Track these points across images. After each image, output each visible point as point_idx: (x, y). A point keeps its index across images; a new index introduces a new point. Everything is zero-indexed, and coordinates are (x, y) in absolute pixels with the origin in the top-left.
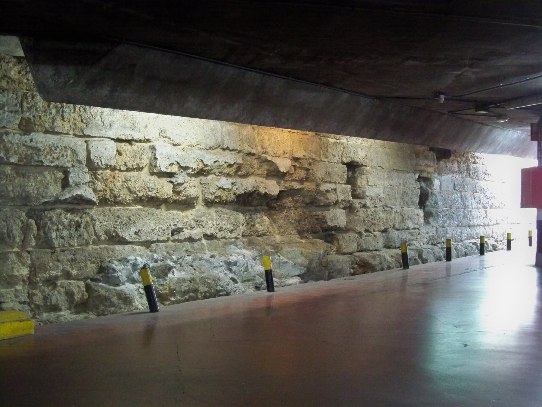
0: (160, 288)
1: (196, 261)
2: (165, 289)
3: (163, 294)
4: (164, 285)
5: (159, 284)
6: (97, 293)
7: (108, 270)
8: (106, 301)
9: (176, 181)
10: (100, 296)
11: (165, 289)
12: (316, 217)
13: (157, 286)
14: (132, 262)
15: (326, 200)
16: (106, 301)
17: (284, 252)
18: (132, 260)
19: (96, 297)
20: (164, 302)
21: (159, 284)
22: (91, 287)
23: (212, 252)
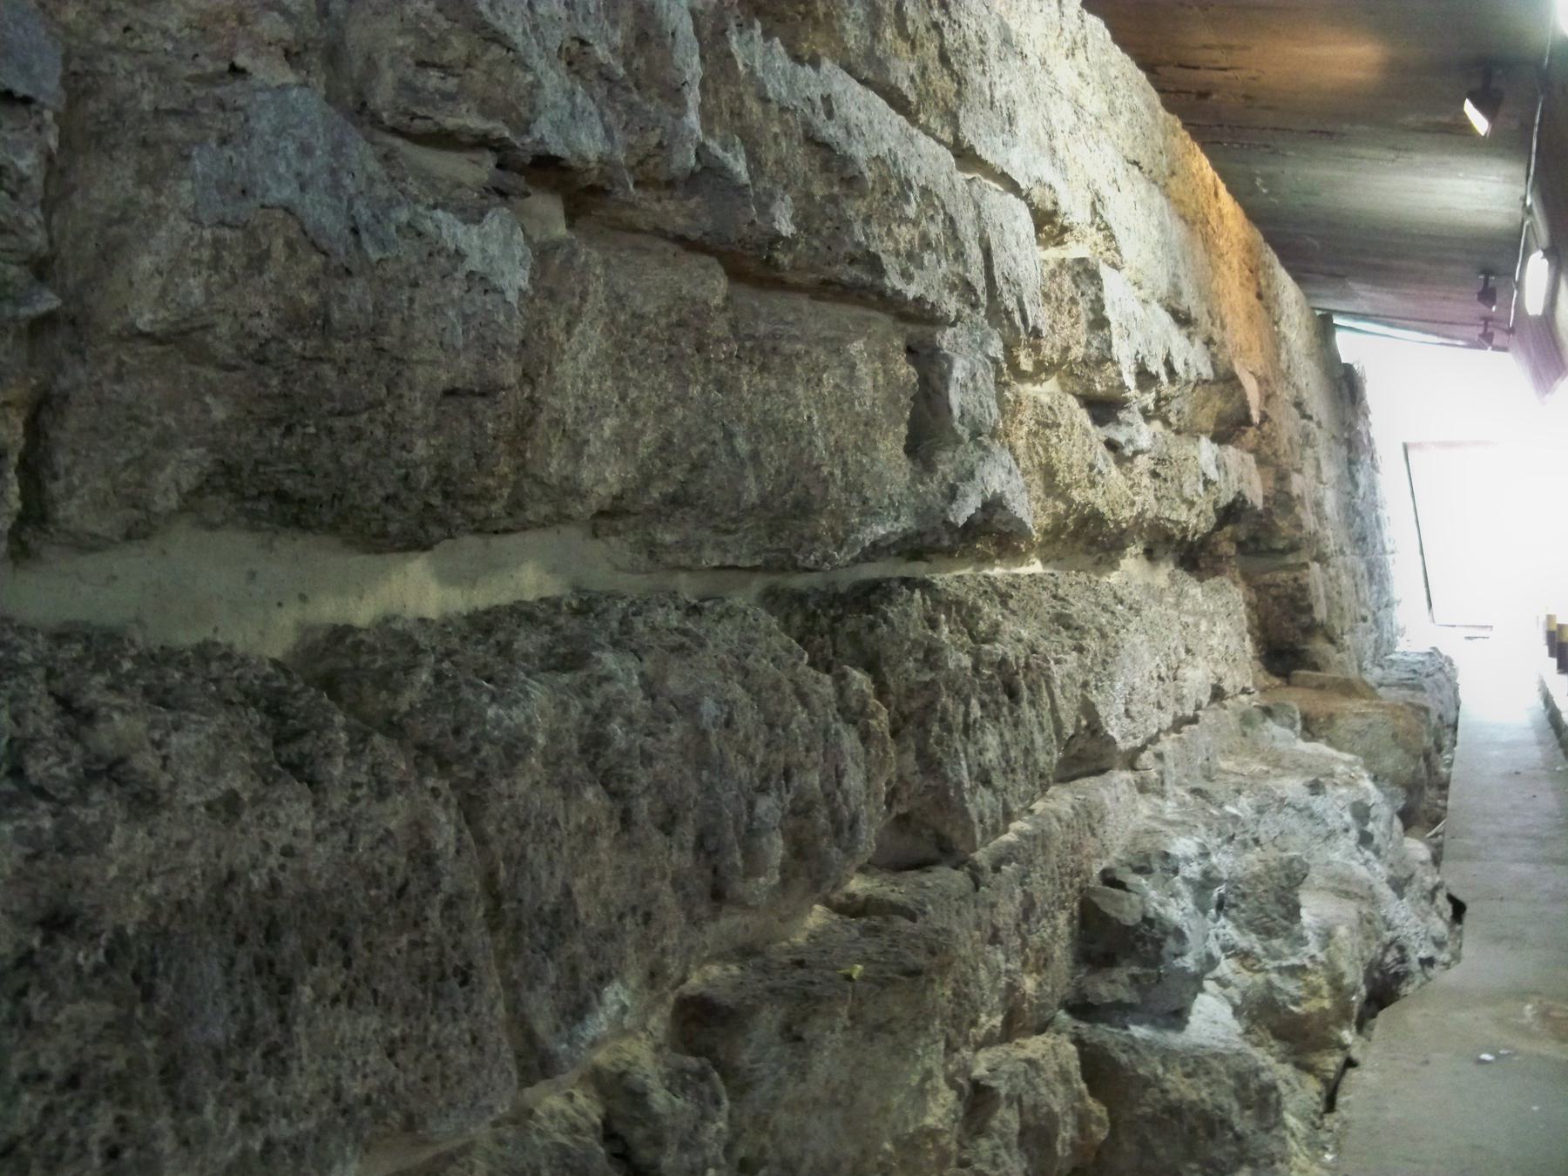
0: (1291, 986)
1: (1267, 817)
2: (1315, 992)
3: (1308, 1016)
4: (1303, 968)
5: (1280, 970)
6: (1153, 1094)
7: (1158, 944)
8: (1211, 1134)
9: (1130, 441)
10: (1175, 1111)
11: (1315, 992)
12: (1274, 591)
13: (1274, 976)
14: (1193, 871)
15: (1293, 531)
16: (1211, 1134)
17: (1341, 733)
18: (1188, 860)
19: (1153, 1120)
20: (1314, 1058)
21: (1280, 970)
22: (1115, 1065)
23: (525, 682)
